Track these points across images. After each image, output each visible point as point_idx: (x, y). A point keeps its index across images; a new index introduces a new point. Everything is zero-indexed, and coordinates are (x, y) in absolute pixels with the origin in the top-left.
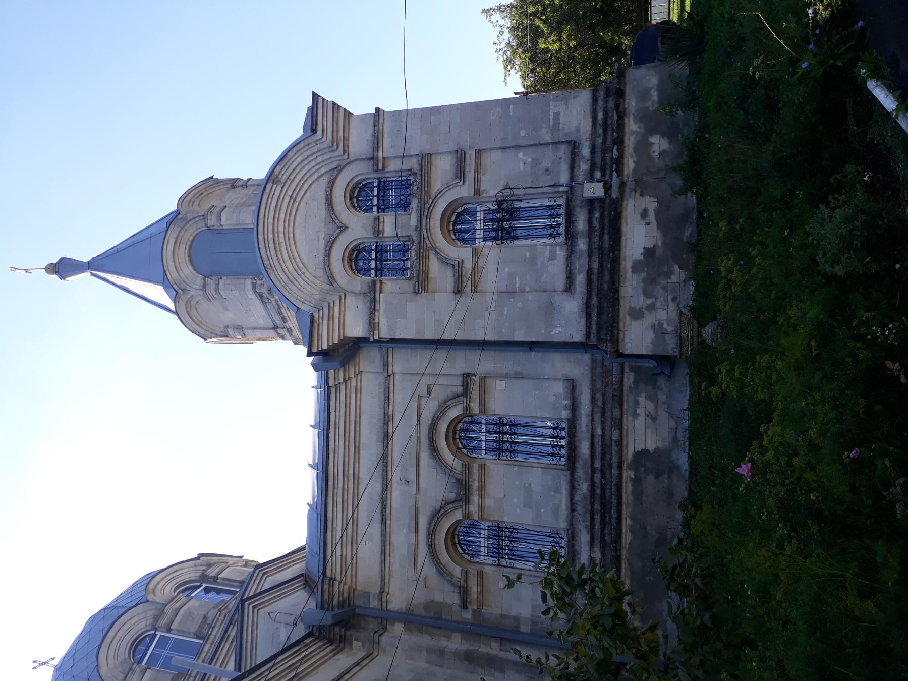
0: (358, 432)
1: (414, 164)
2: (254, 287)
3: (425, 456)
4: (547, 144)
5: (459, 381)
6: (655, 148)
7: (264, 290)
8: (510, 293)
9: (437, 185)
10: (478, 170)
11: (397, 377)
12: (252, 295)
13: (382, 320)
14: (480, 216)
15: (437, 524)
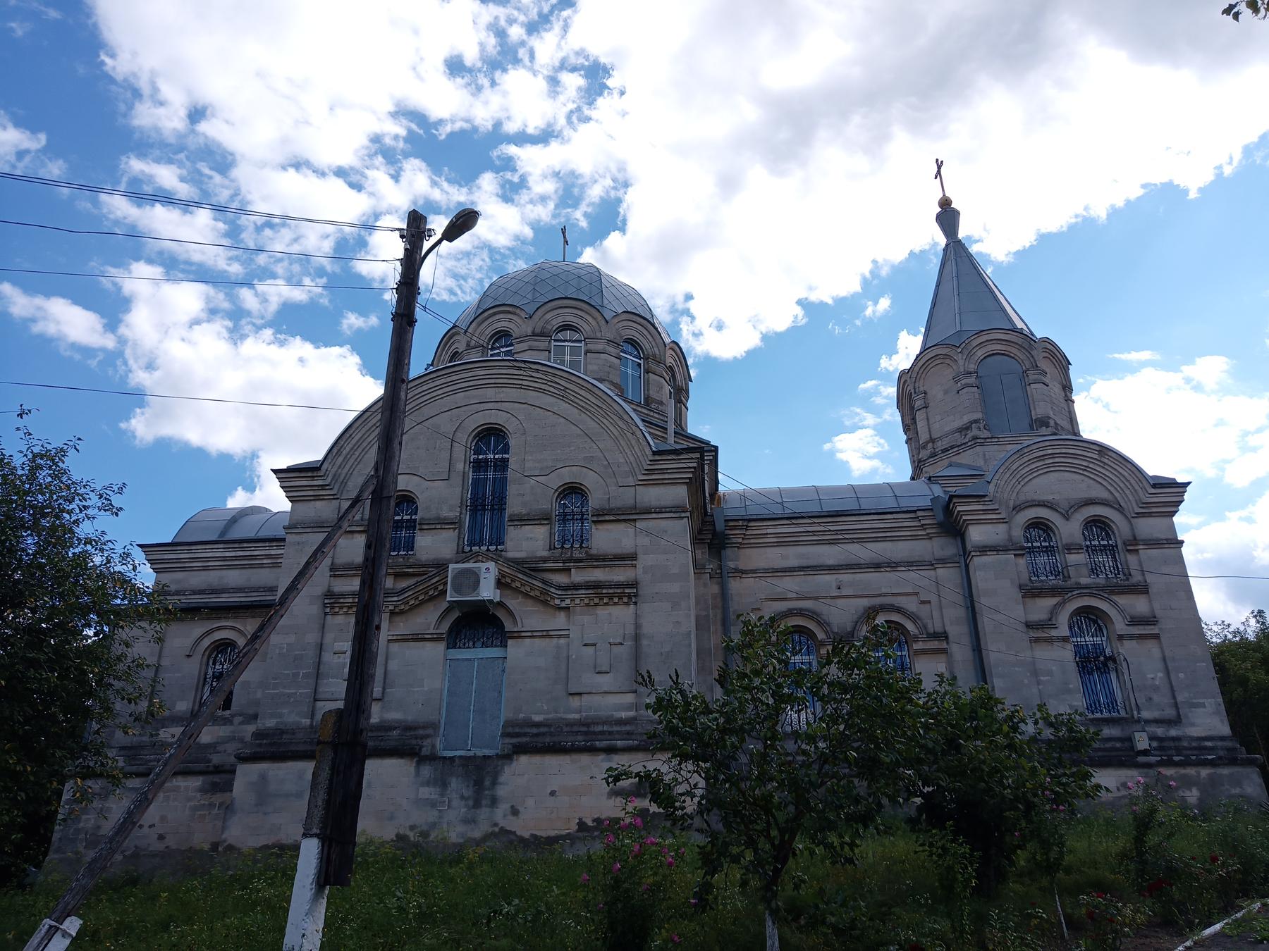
0: (876, 540)
1: (1137, 577)
2: (976, 421)
3: (865, 602)
4: (1174, 697)
5: (939, 629)
6: (1187, 793)
7: (975, 432)
8: (1035, 673)
9: (1122, 600)
10: (1141, 637)
11: (932, 572)
12: (966, 419)
13: (989, 559)
14: (1098, 640)
15: (811, 618)
